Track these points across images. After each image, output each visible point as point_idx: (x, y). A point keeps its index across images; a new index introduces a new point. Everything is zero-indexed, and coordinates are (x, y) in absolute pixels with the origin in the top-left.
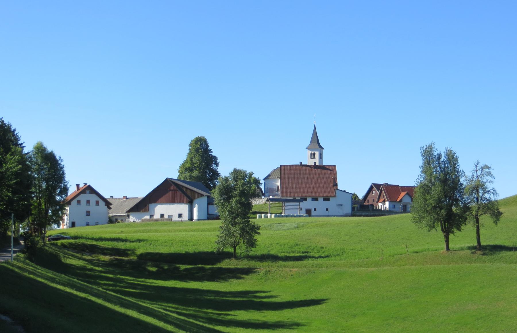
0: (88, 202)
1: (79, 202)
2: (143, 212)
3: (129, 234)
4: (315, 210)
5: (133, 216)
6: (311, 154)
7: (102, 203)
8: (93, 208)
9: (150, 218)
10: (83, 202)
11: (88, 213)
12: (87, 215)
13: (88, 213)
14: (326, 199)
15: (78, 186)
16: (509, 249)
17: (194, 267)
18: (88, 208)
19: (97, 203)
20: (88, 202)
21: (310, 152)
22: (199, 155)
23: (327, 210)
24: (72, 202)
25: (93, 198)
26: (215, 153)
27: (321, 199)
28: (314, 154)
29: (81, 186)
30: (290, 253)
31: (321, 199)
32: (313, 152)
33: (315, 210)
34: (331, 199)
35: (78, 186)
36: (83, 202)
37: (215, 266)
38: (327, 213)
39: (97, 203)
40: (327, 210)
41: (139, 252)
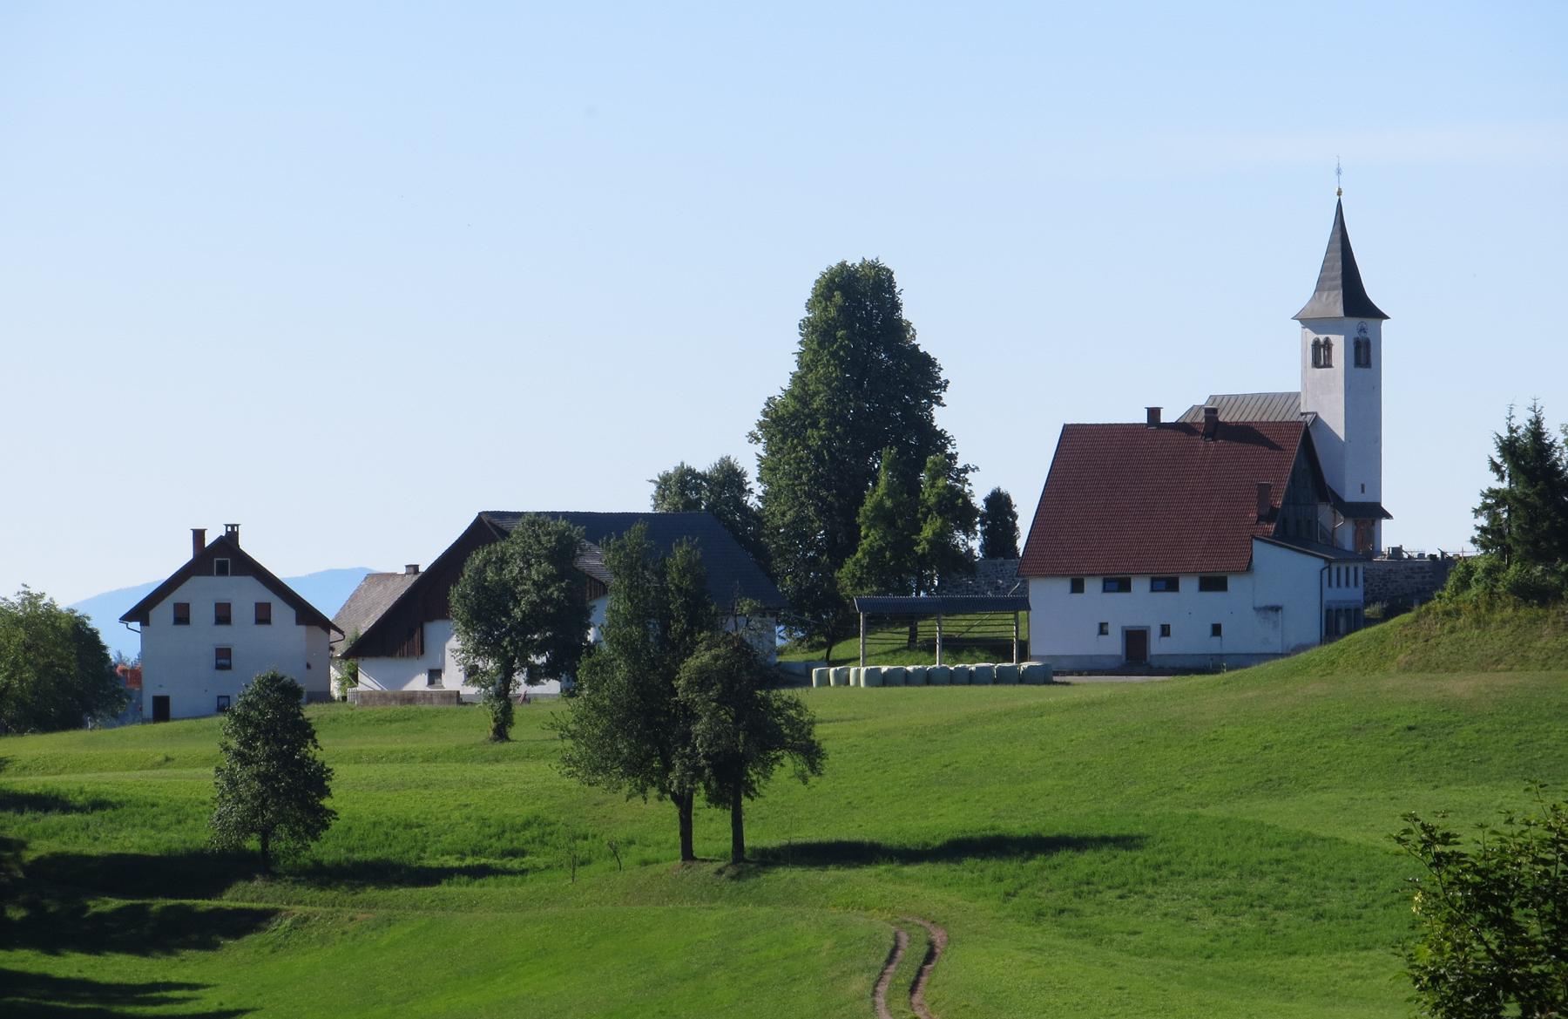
0: (223, 615)
1: (182, 616)
2: (402, 655)
3: (73, 777)
4: (1165, 631)
5: (369, 674)
6: (1316, 344)
7: (282, 613)
8: (242, 634)
9: (431, 683)
10: (202, 613)
11: (223, 658)
12: (219, 667)
13: (223, 658)
14: (1213, 583)
15: (199, 535)
16: (1078, 844)
17: (127, 907)
18: (224, 636)
19: (263, 615)
20: (223, 615)
21: (1311, 336)
22: (834, 355)
23: (1216, 630)
24: (154, 614)
25: (243, 594)
26: (925, 341)
27: (1189, 585)
28: (1328, 345)
29: (209, 540)
30: (463, 855)
31: (1189, 585)
32: (1322, 338)
33: (1165, 631)
34: (1232, 582)
35: (199, 535)
36: (202, 613)
37: (213, 903)
38: (1214, 646)
39: (263, 615)
40: (1216, 630)
41: (40, 848)
